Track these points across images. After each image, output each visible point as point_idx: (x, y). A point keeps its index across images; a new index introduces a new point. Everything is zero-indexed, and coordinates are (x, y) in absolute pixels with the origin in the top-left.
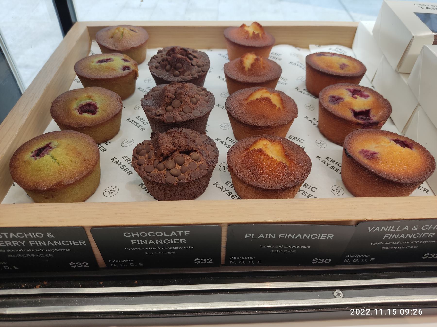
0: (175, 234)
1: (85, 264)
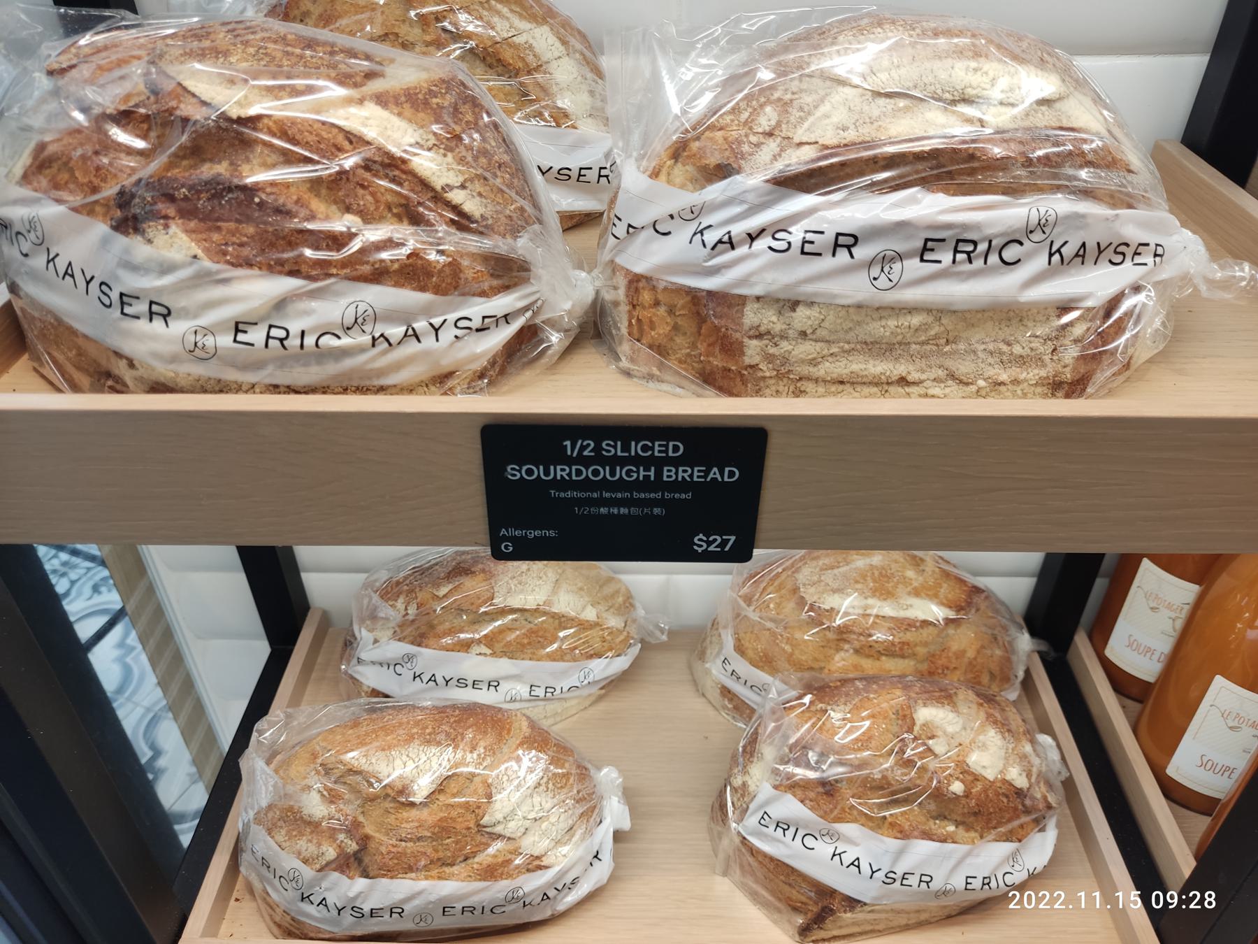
0: (718, 476)
1: (715, 540)
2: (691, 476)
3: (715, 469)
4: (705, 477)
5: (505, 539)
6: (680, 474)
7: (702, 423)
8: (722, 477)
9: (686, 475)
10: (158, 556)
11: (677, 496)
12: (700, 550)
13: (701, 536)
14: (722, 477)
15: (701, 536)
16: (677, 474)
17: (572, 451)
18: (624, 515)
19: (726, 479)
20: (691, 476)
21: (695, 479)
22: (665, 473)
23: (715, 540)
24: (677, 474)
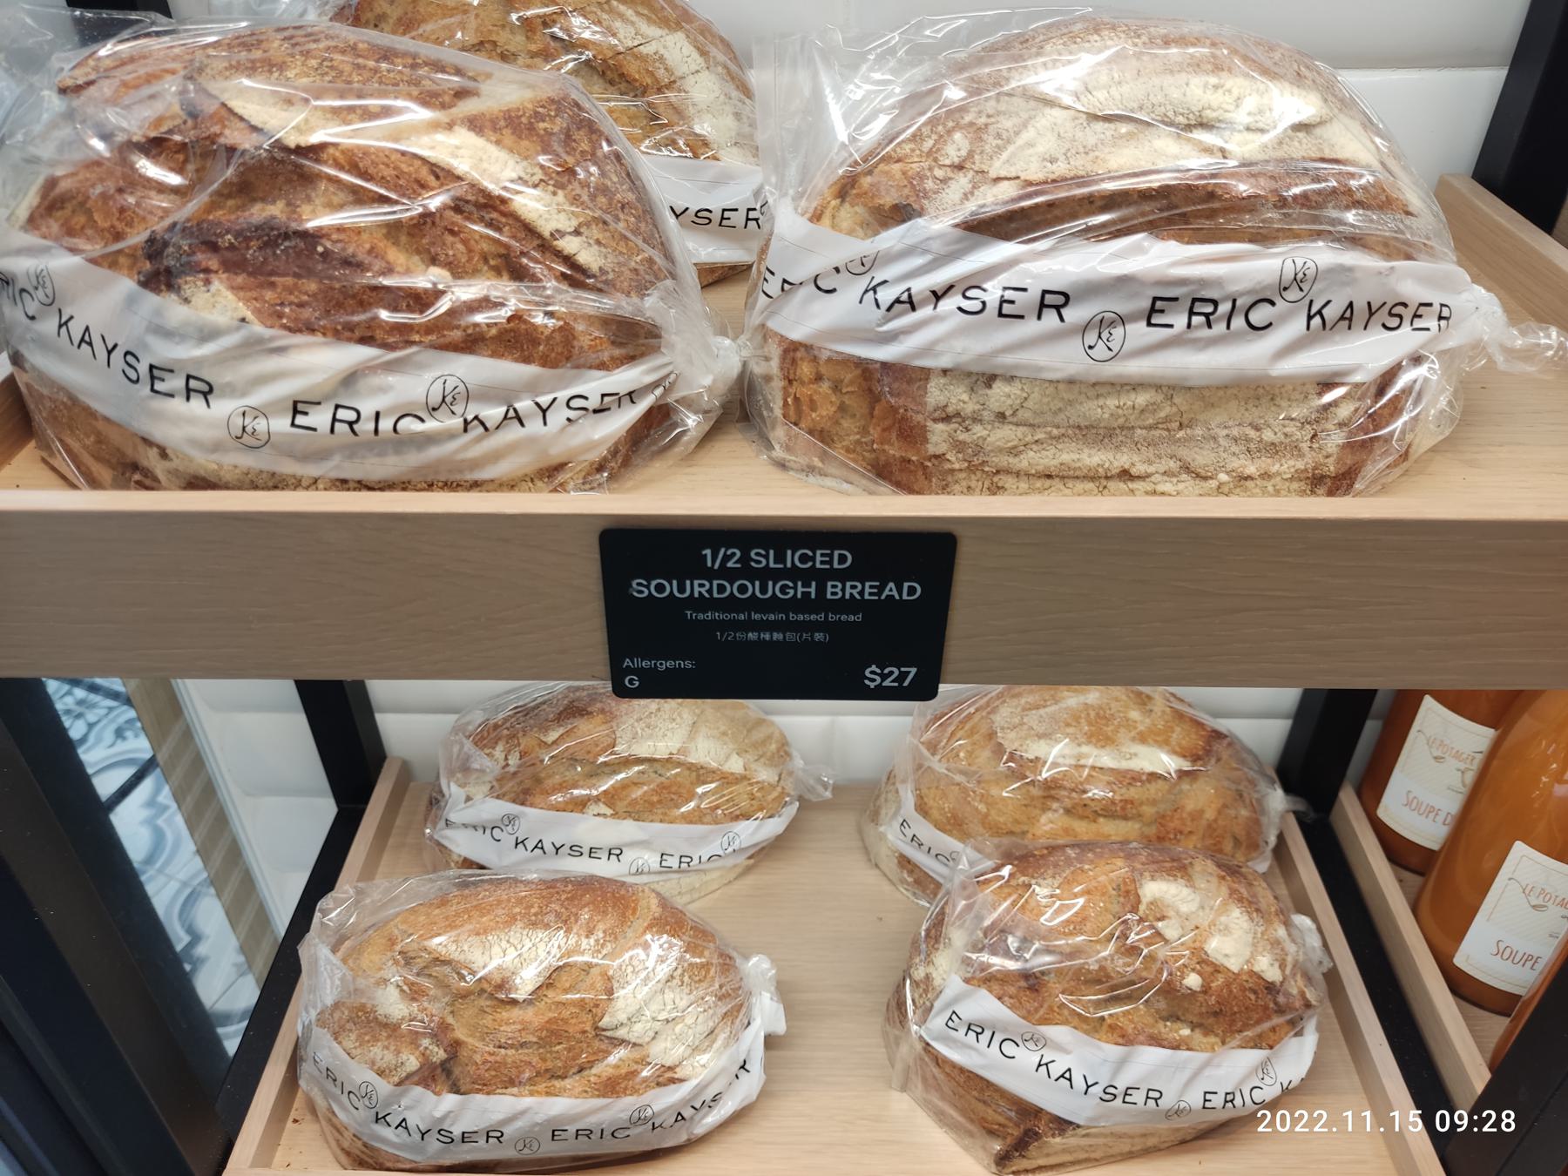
1: (891, 673)
2: (861, 593)
3: (891, 585)
4: (879, 594)
5: (630, 671)
6: (848, 591)
7: (875, 527)
8: (900, 594)
9: (855, 592)
10: (197, 693)
11: (844, 617)
12: (872, 685)
13: (874, 668)
14: (900, 594)
15: (874, 668)
16: (843, 590)
17: (713, 562)
18: (778, 641)
19: (905, 597)
20: (861, 593)
21: (867, 597)
22: (829, 590)
23: (891, 673)
24: (843, 590)
